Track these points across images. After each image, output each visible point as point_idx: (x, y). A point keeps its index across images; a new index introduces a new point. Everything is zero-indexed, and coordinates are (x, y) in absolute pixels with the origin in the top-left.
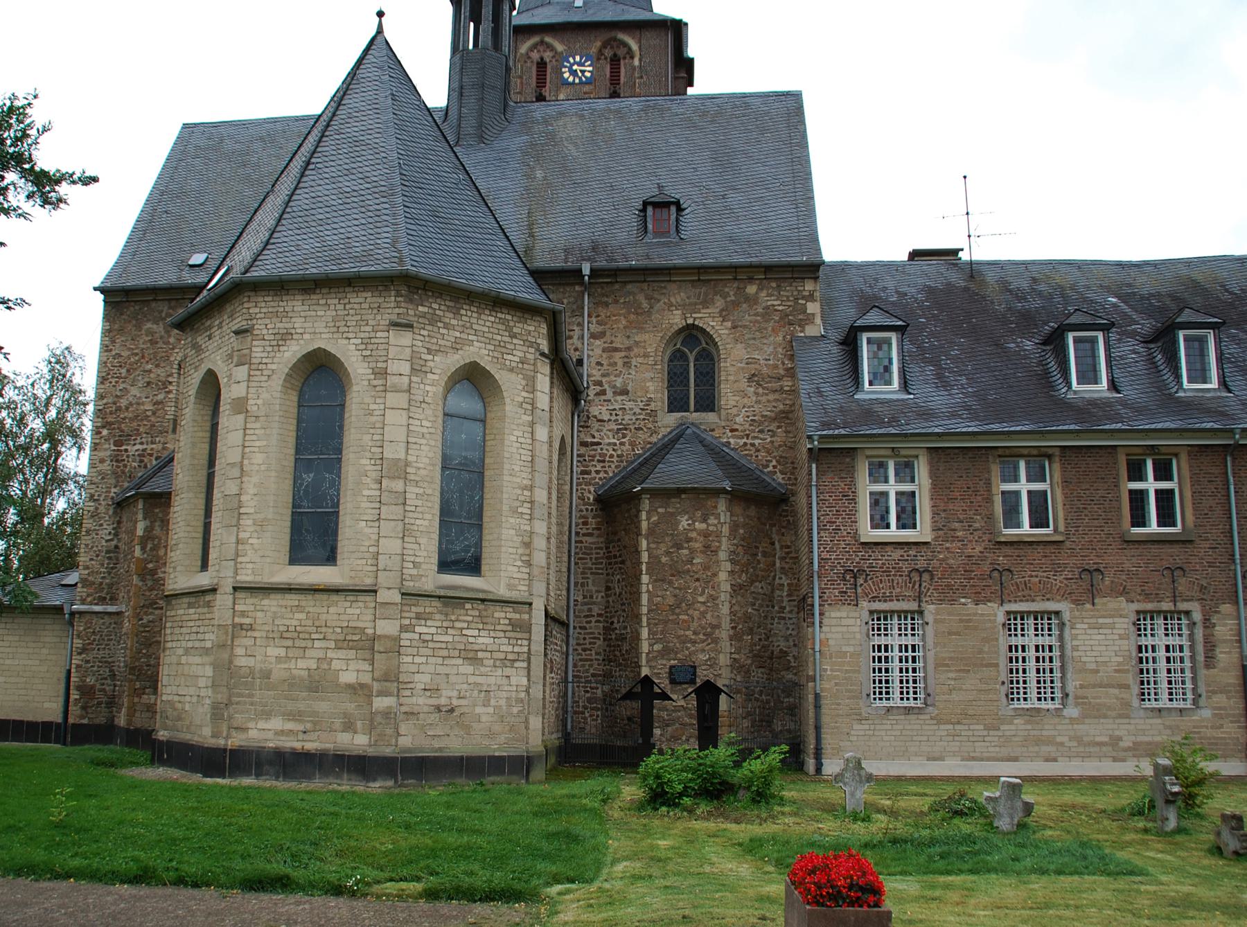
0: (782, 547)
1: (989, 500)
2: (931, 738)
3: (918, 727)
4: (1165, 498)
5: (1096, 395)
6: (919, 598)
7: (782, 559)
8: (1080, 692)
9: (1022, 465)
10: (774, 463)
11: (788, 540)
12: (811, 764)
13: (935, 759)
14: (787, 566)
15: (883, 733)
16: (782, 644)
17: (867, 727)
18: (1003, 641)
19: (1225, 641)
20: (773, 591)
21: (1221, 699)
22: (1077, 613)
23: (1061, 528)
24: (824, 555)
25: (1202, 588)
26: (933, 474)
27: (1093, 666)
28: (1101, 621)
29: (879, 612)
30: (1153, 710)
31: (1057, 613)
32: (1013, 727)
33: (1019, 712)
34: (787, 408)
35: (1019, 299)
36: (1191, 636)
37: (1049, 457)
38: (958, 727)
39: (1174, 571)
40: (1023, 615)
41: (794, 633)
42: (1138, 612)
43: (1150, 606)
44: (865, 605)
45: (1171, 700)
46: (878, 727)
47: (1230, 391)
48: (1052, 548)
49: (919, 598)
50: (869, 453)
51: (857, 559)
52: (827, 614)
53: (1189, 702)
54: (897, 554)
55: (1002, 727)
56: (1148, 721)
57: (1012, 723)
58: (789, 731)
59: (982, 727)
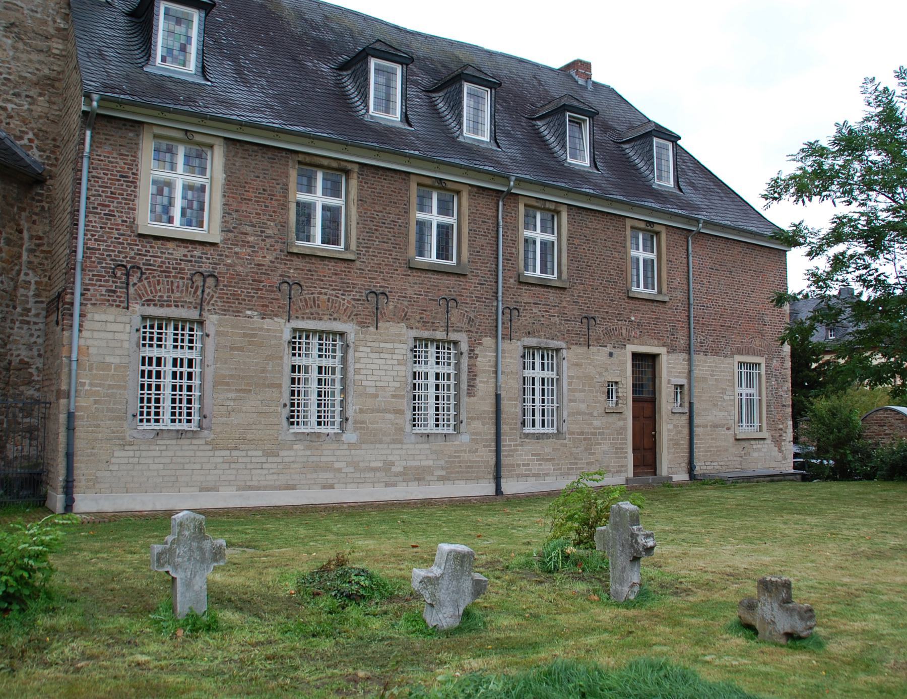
0: (31, 237)
1: (284, 206)
2: (205, 466)
3: (191, 453)
4: (444, 231)
5: (390, 124)
6: (200, 306)
7: (31, 251)
8: (360, 417)
9: (320, 176)
10: (31, 136)
11: (39, 229)
12: (58, 500)
13: (208, 489)
14: (37, 261)
15: (150, 461)
16: (24, 353)
17: (131, 454)
18: (288, 361)
19: (484, 372)
20: (15, 288)
21: (477, 425)
22: (361, 336)
23: (353, 247)
24: (91, 244)
25: (470, 320)
26: (229, 169)
27: (372, 391)
28: (382, 345)
29: (153, 318)
30: (422, 435)
31: (342, 334)
32: (292, 453)
33: (299, 437)
34: (54, 74)
35: (314, 29)
36: (458, 366)
37: (347, 172)
38: (234, 453)
39: (450, 302)
40: (308, 333)
41: (40, 341)
42: (416, 339)
43: (426, 334)
44: (138, 309)
45: (437, 426)
46: (144, 454)
47: (499, 147)
48: (341, 266)
49: (200, 306)
50: (157, 131)
51: (132, 254)
52: (89, 316)
53: (452, 427)
54: (180, 252)
55: (282, 453)
56: (418, 446)
57: (291, 449)
58: (28, 458)
59: (260, 453)
